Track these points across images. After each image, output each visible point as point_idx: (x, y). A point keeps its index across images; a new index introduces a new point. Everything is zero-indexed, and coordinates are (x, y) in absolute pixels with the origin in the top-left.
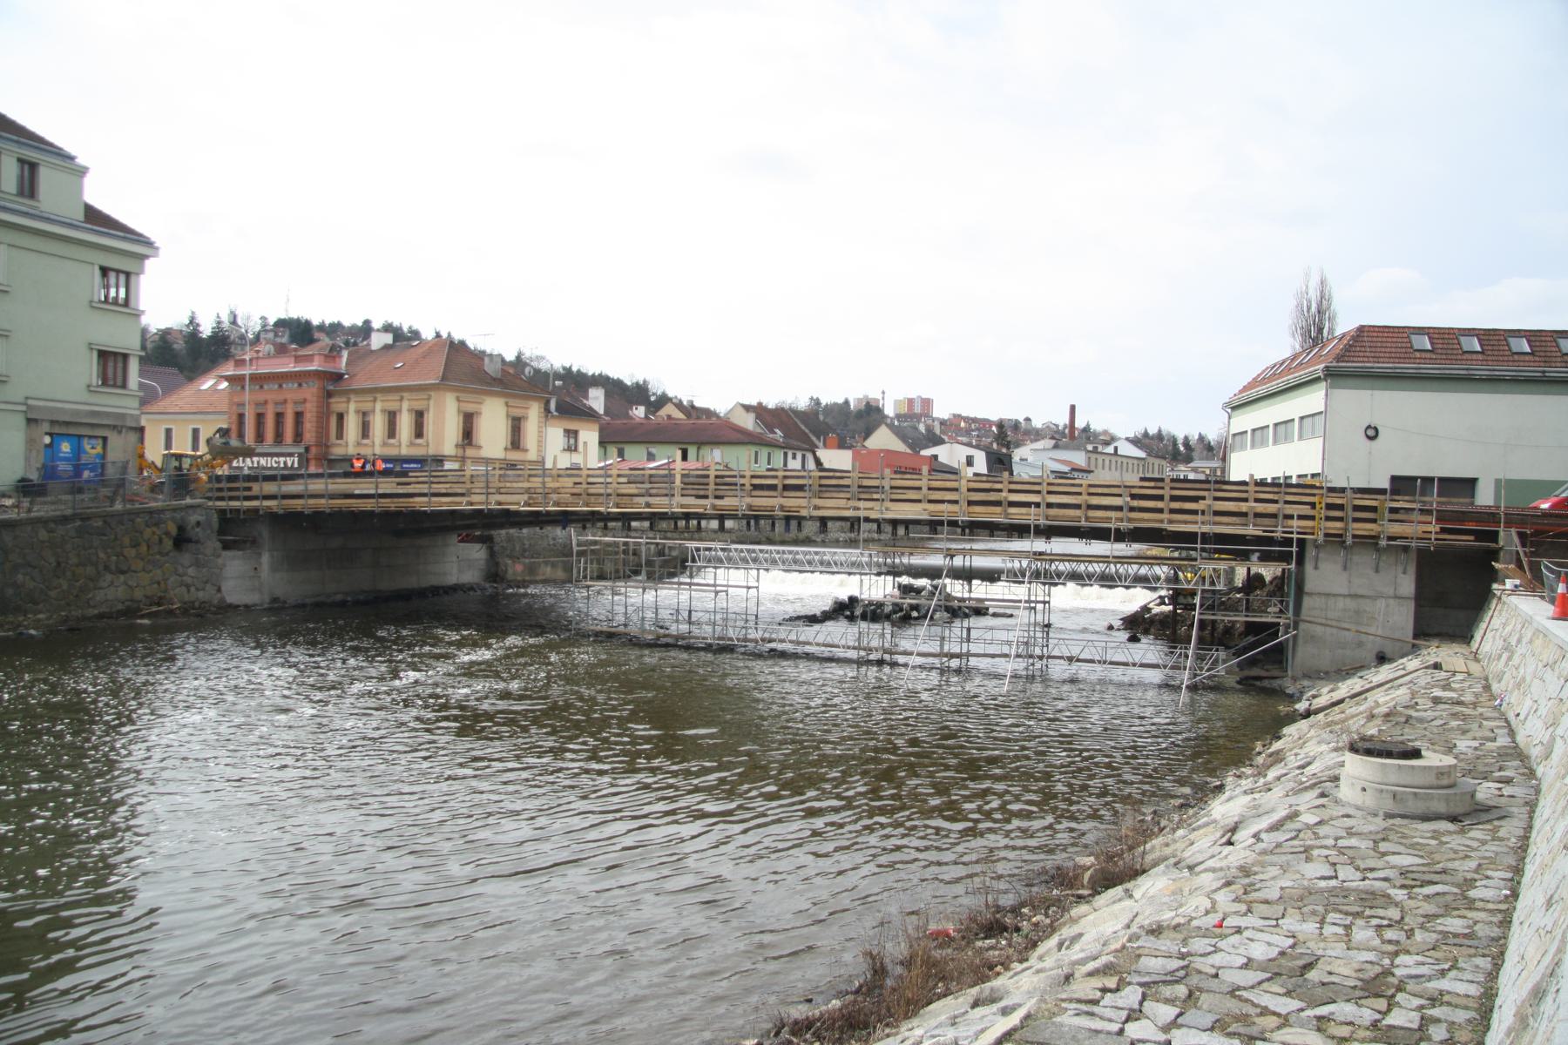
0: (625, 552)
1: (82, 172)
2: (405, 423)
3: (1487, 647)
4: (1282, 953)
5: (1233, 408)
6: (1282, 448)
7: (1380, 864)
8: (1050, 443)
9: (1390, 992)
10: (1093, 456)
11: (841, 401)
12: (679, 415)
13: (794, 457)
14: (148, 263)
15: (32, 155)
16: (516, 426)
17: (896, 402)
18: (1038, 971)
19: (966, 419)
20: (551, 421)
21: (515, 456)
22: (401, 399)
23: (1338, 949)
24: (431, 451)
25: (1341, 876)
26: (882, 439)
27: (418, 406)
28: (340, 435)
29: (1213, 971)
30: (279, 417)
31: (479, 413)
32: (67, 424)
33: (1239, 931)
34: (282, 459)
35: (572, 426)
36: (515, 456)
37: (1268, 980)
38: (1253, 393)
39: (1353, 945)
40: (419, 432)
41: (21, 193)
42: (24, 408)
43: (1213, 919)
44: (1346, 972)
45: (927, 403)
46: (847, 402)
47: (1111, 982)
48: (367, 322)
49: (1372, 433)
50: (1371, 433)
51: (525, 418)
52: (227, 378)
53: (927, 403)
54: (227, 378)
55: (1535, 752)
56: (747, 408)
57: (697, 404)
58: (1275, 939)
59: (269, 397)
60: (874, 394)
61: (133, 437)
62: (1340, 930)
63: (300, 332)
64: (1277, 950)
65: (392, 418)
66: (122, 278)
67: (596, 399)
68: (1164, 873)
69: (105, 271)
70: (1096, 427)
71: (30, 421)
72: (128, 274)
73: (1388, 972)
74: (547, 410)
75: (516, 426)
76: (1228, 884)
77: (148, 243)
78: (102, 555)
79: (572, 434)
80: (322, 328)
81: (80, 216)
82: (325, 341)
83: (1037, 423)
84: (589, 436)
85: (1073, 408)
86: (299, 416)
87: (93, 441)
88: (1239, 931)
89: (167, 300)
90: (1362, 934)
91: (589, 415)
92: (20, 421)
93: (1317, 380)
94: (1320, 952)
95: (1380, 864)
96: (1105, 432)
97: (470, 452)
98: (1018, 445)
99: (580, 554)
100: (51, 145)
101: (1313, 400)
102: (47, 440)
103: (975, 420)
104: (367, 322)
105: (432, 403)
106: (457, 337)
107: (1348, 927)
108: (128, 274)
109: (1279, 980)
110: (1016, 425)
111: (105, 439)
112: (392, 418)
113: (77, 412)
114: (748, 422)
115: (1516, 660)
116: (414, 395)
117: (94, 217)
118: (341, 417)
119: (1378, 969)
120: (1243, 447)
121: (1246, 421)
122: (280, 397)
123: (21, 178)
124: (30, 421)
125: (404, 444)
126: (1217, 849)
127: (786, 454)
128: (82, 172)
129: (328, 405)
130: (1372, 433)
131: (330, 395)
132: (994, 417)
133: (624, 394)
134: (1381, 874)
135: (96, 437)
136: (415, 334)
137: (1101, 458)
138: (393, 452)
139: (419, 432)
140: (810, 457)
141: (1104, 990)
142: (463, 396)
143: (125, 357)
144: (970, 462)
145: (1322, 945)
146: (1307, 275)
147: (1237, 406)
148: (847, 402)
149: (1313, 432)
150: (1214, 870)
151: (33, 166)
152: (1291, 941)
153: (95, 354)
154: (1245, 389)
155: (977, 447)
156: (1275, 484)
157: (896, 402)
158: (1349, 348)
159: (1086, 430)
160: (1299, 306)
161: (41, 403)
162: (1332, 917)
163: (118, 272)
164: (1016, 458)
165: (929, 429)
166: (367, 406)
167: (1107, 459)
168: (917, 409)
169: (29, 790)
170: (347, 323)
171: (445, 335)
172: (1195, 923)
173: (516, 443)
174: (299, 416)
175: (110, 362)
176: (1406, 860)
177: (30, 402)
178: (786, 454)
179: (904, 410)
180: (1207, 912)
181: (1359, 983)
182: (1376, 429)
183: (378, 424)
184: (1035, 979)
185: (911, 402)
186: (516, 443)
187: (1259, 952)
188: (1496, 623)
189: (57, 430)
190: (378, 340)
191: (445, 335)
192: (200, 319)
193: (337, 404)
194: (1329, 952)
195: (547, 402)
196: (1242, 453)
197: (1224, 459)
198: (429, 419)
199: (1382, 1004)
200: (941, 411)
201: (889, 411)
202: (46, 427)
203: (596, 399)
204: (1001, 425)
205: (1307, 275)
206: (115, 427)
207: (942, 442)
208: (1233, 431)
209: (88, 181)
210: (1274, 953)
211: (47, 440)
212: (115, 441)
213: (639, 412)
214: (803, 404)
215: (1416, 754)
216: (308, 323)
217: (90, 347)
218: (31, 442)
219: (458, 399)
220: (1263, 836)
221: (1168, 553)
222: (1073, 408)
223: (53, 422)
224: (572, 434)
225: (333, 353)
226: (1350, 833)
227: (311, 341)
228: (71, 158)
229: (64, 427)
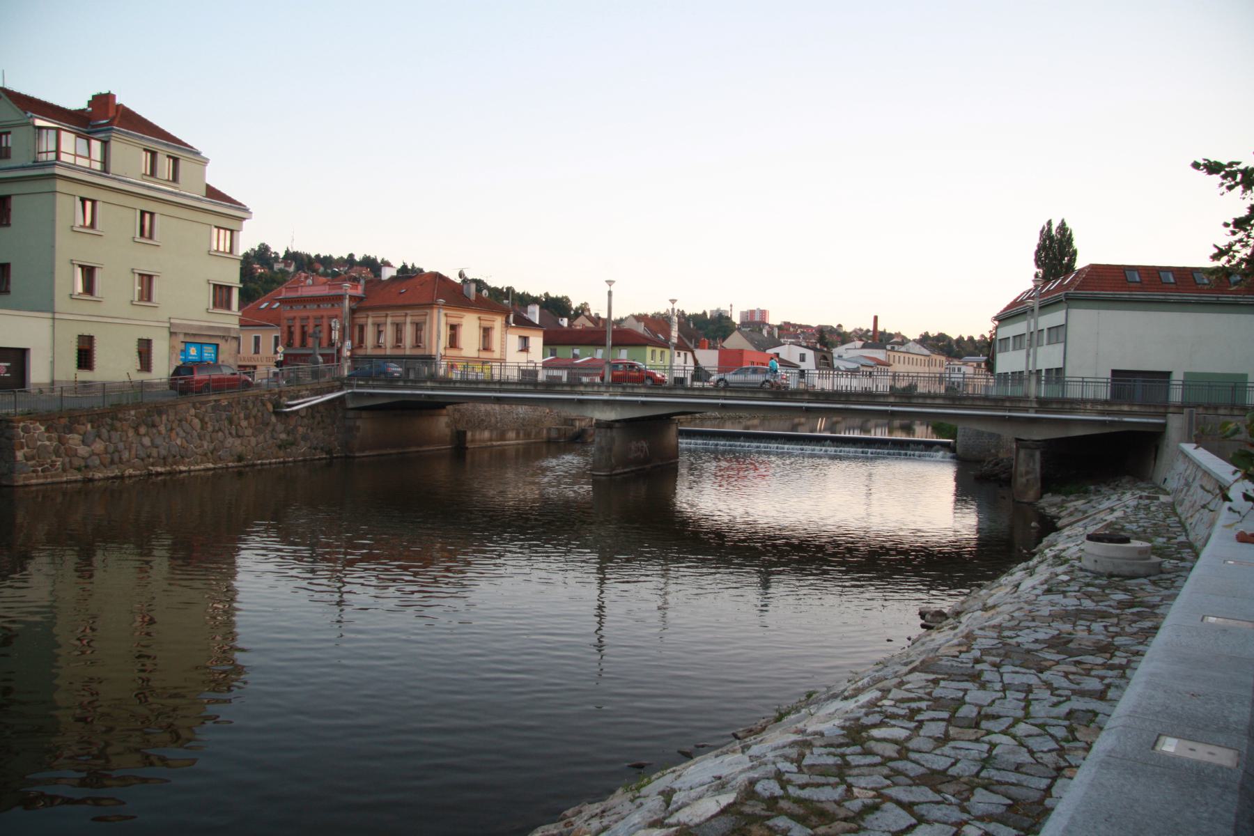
1: (205, 162)
2: (408, 332)
3: (1172, 484)
10: (892, 354)
11: (700, 312)
12: (590, 324)
14: (245, 223)
16: (486, 332)
17: (742, 313)
20: (510, 330)
21: (485, 355)
26: (735, 341)
27: (417, 319)
31: (459, 325)
33: (1028, 628)
35: (525, 333)
36: (485, 355)
45: (763, 313)
46: (705, 313)
47: (964, 649)
53: (763, 313)
55: (1198, 544)
58: (1048, 631)
59: (325, 314)
60: (724, 307)
65: (398, 328)
66: (228, 233)
67: (534, 313)
74: (507, 322)
75: (486, 332)
77: (246, 210)
79: (525, 339)
83: (848, 328)
84: (536, 341)
85: (876, 318)
88: (1028, 628)
96: (898, 335)
98: (835, 346)
100: (186, 145)
102: (183, 347)
103: (801, 326)
110: (832, 331)
111: (217, 345)
112: (398, 328)
113: (201, 328)
114: (641, 328)
115: (1192, 490)
117: (212, 193)
120: (1006, 350)
121: (1010, 330)
122: (318, 314)
124: (172, 334)
128: (205, 162)
132: (815, 324)
133: (555, 306)
137: (897, 355)
140: (689, 355)
141: (961, 652)
143: (229, 288)
144: (803, 358)
147: (1004, 318)
148: (705, 313)
153: (137, 277)
155: (807, 347)
165: (770, 333)
167: (902, 355)
168: (757, 318)
170: (336, 257)
173: (486, 347)
183: (389, 332)
185: (752, 312)
186: (486, 347)
187: (1041, 635)
190: (387, 273)
195: (508, 317)
199: (1108, 655)
200: (774, 319)
201: (736, 319)
202: (182, 338)
203: (534, 313)
208: (1000, 337)
211: (183, 347)
212: (224, 346)
213: (565, 322)
218: (172, 348)
219: (446, 315)
222: (876, 318)
223: (186, 334)
224: (525, 339)
226: (1088, 585)
228: (198, 153)
229: (193, 337)
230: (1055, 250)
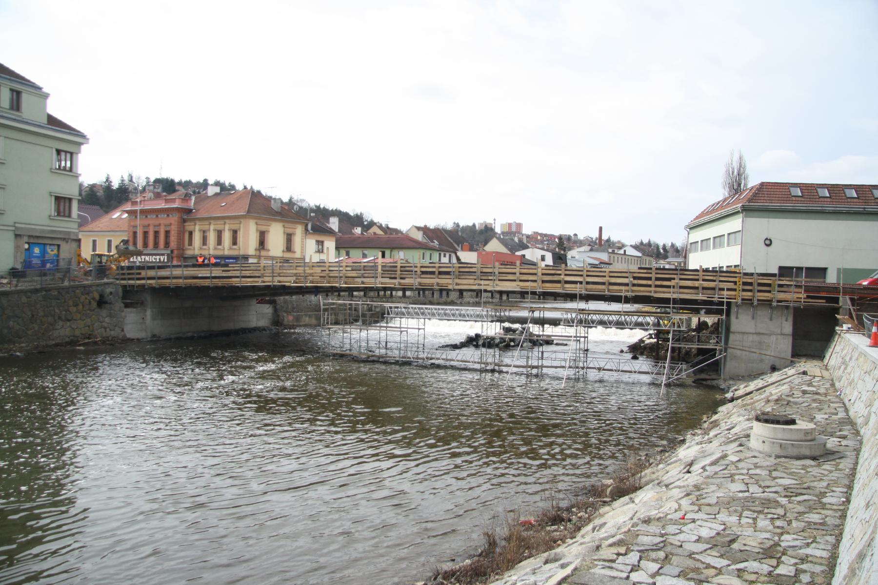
0: (350, 309)
1: (46, 96)
2: (227, 237)
3: (832, 362)
4: (718, 534)
5: (691, 229)
6: (718, 251)
7: (773, 483)
8: (588, 248)
9: (778, 556)
10: (612, 255)
11: (471, 224)
12: (380, 232)
13: (445, 256)
14: (83, 147)
15: (18, 87)
16: (289, 238)
17: (502, 225)
18: (581, 544)
19: (541, 235)
20: (309, 236)
21: (288, 255)
22: (225, 224)
23: (749, 531)
24: (242, 253)
25: (751, 490)
26: (494, 246)
27: (234, 227)
28: (190, 244)
29: (679, 544)
30: (156, 233)
31: (268, 231)
32: (38, 237)
33: (694, 521)
34: (158, 257)
35: (320, 238)
36: (288, 255)
37: (710, 548)
38: (702, 220)
39: (757, 529)
40: (235, 242)
41: (12, 108)
42: (13, 228)
43: (679, 514)
44: (754, 544)
45: (519, 226)
46: (474, 225)
47: (622, 550)
48: (206, 181)
49: (768, 243)
50: (768, 242)
51: (294, 234)
52: (127, 212)
53: (519, 226)
54: (127, 212)
55: (859, 421)
56: (419, 228)
57: (391, 226)
58: (714, 526)
59: (151, 222)
60: (490, 221)
61: (74, 245)
62: (751, 521)
63: (168, 186)
64: (715, 532)
65: (219, 234)
66: (68, 156)
67: (334, 224)
68: (652, 489)
69: (59, 152)
70: (614, 239)
71: (17, 236)
72: (72, 154)
73: (777, 544)
74: (306, 230)
75: (289, 238)
76: (688, 495)
77: (83, 136)
78: (57, 311)
79: (320, 243)
80: (180, 183)
81: (45, 121)
82: (182, 191)
83: (581, 237)
84: (330, 244)
85: (601, 228)
86: (167, 233)
87: (52, 247)
88: (694, 521)
89: (93, 168)
90: (763, 523)
91: (330, 232)
92: (11, 235)
93: (738, 213)
94: (739, 533)
95: (773, 483)
96: (619, 242)
97: (263, 253)
98: (570, 249)
99: (325, 310)
100: (29, 81)
101: (735, 224)
102: (26, 246)
103: (546, 235)
104: (206, 181)
105: (242, 225)
106: (256, 189)
107: (755, 519)
108: (72, 154)
109: (716, 549)
110: (569, 238)
111: (59, 246)
112: (219, 234)
113: (43, 231)
114: (419, 236)
116: (232, 221)
117: (53, 121)
118: (191, 233)
119: (772, 543)
120: (696, 250)
121: (698, 235)
122: (157, 222)
123: (12, 99)
124: (17, 236)
125: (226, 249)
126: (681, 475)
127: (440, 254)
128: (46, 96)
129: (184, 227)
130: (768, 243)
131: (185, 221)
132: (557, 233)
134: (773, 489)
135: (54, 245)
136: (233, 187)
137: (616, 257)
138: (220, 253)
139: (235, 242)
140: (453, 256)
141: (618, 554)
142: (259, 222)
143: (70, 200)
144: (543, 258)
145: (740, 529)
146: (732, 154)
147: (693, 228)
148: (474, 225)
149: (735, 242)
150: (680, 487)
151: (18, 93)
152: (723, 527)
153: (53, 198)
154: (697, 218)
155: (547, 250)
156: (714, 271)
157: (502, 225)
158: (755, 195)
159: (608, 240)
160: (727, 171)
161: (23, 226)
162: (746, 513)
163: (66, 152)
164: (569, 256)
165: (520, 240)
166: (205, 227)
167: (620, 257)
168: (514, 229)
169: (16, 442)
170: (194, 181)
171: (249, 188)
172: (669, 517)
173: (289, 248)
174: (167, 233)
175: (62, 203)
176: (787, 482)
177: (17, 225)
178: (440, 254)
179: (506, 230)
180: (676, 511)
181: (761, 551)
182: (770, 240)
183: (212, 237)
184: (580, 548)
185: (510, 225)
186: (289, 248)
187: (705, 533)
188: (838, 349)
189: (32, 241)
190: (212, 191)
191: (249, 188)
192: (112, 179)
193: (189, 226)
194: (744, 533)
195: (307, 225)
196: (696, 254)
197: (685, 257)
198: (240, 235)
199: (774, 562)
200: (527, 230)
201: (498, 230)
202: (26, 239)
203: (334, 224)
204: (560, 238)
205: (732, 154)
206: (64, 239)
207: (527, 247)
208: (690, 241)
209: (49, 102)
210: (713, 533)
211: (26, 246)
212: (64, 247)
213: (358, 230)
214: (449, 226)
215: (793, 422)
216: (172, 181)
217: (51, 194)
218: (17, 247)
219: (256, 224)
220: (707, 468)
221: (654, 310)
222: (601, 228)
223: (30, 236)
224: (320, 243)
225: (186, 198)
226: (756, 466)
227: (174, 191)
228: (40, 89)
229: (36, 239)
230: (736, 185)
